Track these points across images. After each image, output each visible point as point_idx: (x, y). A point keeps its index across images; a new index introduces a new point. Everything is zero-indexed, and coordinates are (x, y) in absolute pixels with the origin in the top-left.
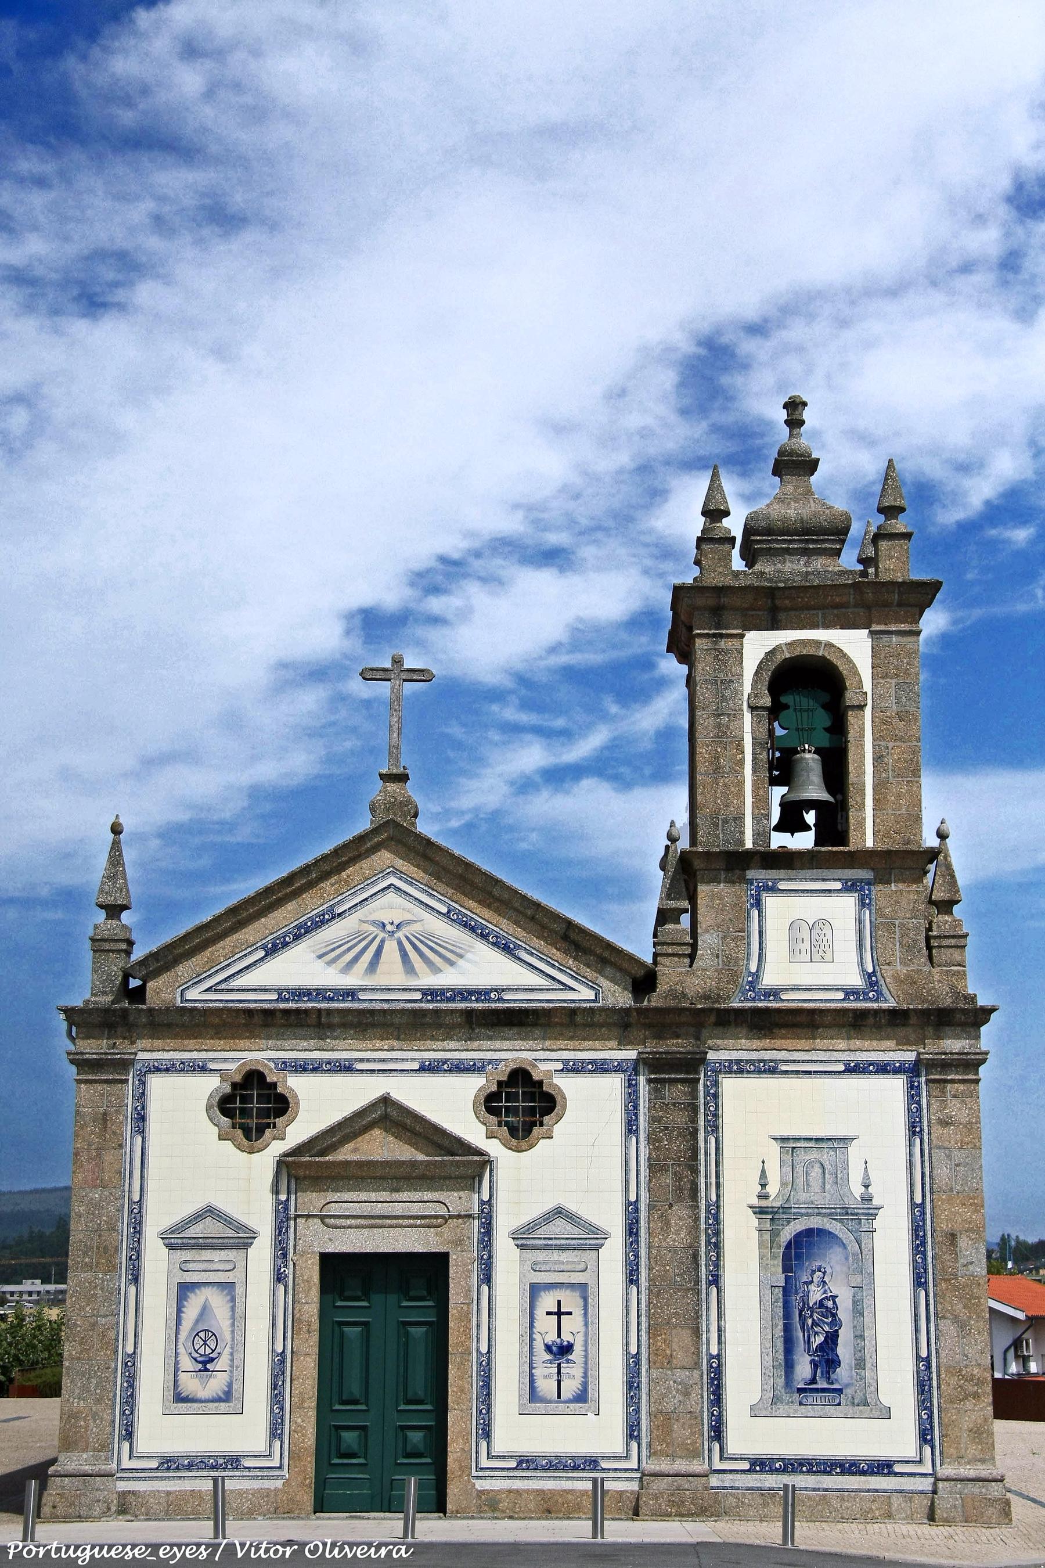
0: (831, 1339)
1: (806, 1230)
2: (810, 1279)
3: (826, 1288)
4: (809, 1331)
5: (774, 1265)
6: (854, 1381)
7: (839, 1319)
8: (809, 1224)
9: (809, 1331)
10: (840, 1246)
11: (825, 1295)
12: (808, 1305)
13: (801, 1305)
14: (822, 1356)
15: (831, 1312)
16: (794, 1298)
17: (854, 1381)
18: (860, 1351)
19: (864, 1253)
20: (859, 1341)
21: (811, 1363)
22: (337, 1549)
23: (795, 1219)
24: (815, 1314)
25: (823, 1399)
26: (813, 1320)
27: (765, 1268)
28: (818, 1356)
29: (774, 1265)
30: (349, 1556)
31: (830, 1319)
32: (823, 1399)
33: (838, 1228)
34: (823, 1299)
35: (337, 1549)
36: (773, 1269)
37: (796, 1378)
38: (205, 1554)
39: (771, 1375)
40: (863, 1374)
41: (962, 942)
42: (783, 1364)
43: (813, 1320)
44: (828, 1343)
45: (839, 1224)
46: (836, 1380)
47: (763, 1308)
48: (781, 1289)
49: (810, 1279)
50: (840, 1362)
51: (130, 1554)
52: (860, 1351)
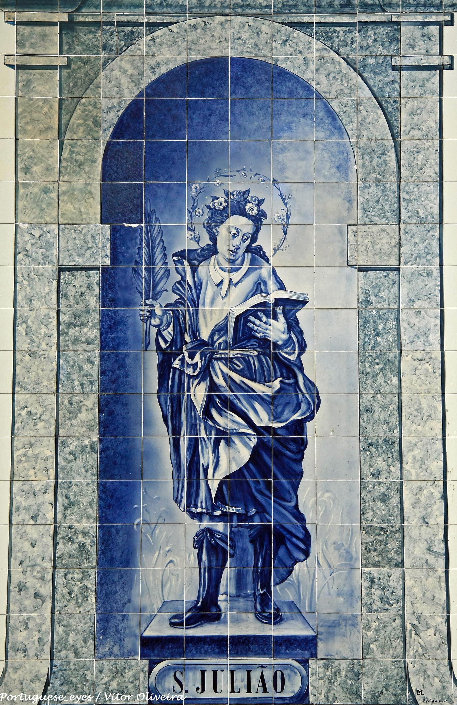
0: (278, 455)
1: (194, 65)
2: (206, 241)
3: (265, 272)
4: (194, 429)
5: (70, 193)
6: (358, 609)
7: (310, 384)
8: (205, 42)
9: (194, 429)
10: (317, 123)
11: (258, 299)
12: (195, 333)
13: (168, 333)
14: (242, 518)
15: (277, 358)
16: (143, 310)
17: (358, 609)
18: (385, 498)
19: (406, 146)
20: (380, 463)
21: (198, 545)
22: (151, 697)
23: (152, 26)
24: (219, 366)
25: (240, 676)
26: (213, 387)
27: (37, 202)
28: (225, 517)
29: (70, 193)
30: (157, 699)
31: (276, 384)
32: (240, 676)
33: (313, 56)
34: (247, 313)
35: (151, 697)
36: (68, 207)
37: (139, 601)
38: (91, 699)
39: (46, 590)
40: (394, 583)
41: (393, 660)
42: (93, 550)
43: (213, 387)
44: (265, 472)
45: (317, 45)
46: (292, 605)
47: (23, 345)
48: (95, 277)
49: (206, 241)
50: (307, 539)
51: (56, 699)
52: (385, 498)
